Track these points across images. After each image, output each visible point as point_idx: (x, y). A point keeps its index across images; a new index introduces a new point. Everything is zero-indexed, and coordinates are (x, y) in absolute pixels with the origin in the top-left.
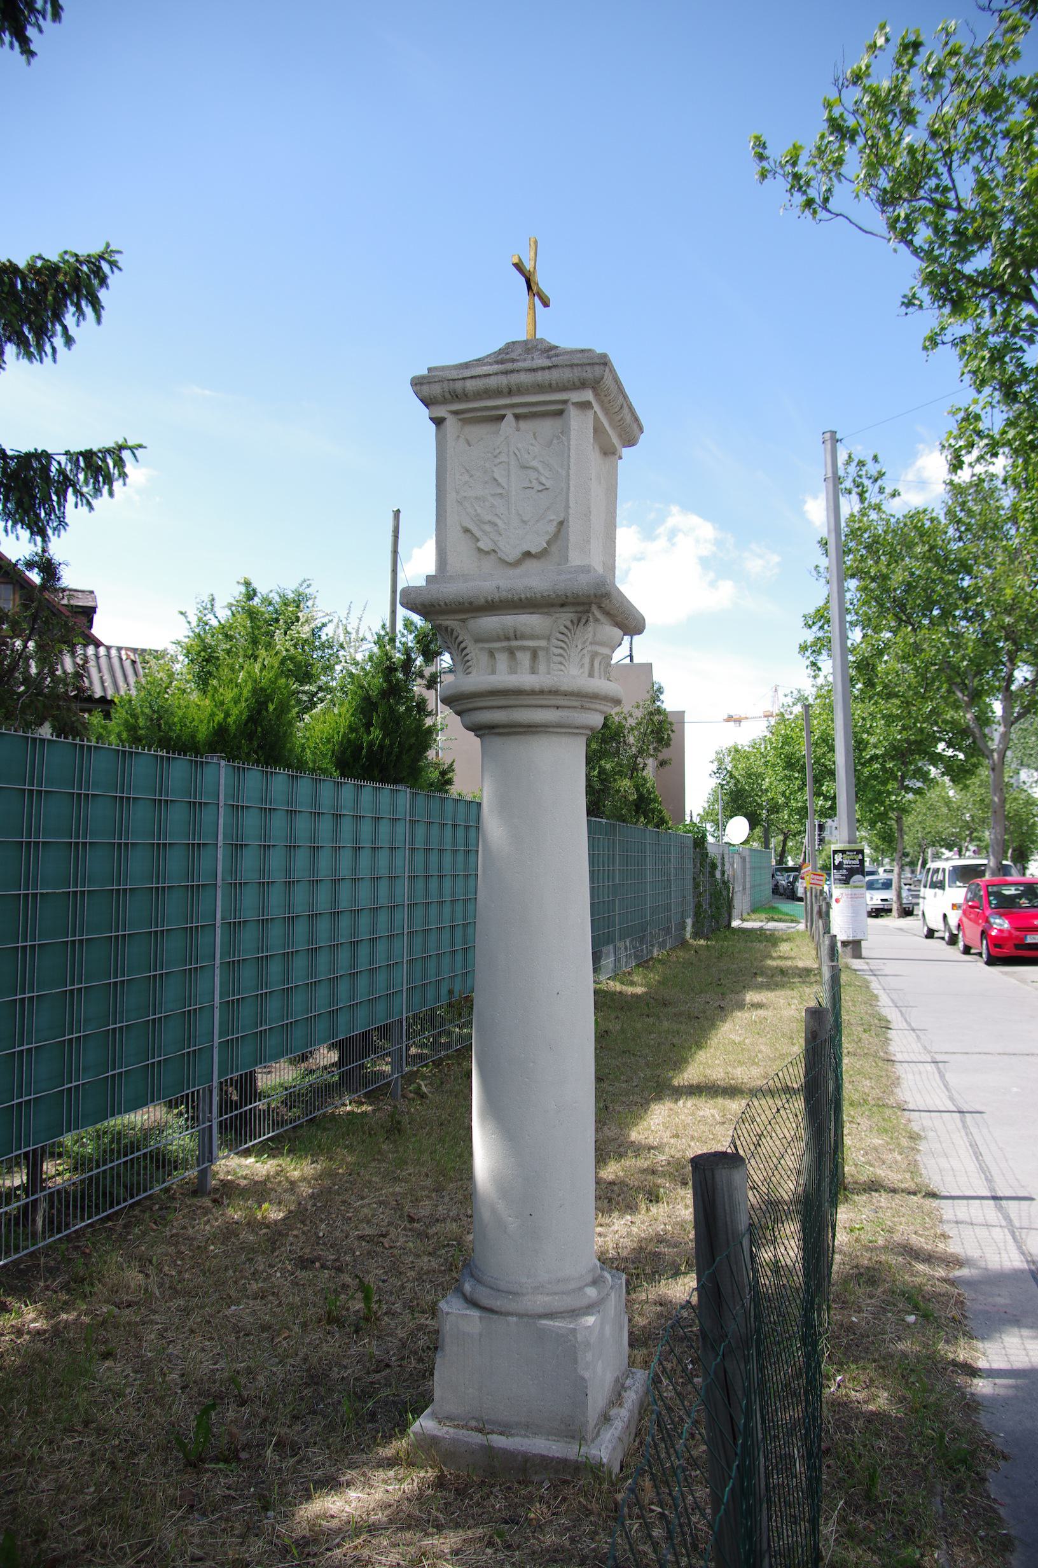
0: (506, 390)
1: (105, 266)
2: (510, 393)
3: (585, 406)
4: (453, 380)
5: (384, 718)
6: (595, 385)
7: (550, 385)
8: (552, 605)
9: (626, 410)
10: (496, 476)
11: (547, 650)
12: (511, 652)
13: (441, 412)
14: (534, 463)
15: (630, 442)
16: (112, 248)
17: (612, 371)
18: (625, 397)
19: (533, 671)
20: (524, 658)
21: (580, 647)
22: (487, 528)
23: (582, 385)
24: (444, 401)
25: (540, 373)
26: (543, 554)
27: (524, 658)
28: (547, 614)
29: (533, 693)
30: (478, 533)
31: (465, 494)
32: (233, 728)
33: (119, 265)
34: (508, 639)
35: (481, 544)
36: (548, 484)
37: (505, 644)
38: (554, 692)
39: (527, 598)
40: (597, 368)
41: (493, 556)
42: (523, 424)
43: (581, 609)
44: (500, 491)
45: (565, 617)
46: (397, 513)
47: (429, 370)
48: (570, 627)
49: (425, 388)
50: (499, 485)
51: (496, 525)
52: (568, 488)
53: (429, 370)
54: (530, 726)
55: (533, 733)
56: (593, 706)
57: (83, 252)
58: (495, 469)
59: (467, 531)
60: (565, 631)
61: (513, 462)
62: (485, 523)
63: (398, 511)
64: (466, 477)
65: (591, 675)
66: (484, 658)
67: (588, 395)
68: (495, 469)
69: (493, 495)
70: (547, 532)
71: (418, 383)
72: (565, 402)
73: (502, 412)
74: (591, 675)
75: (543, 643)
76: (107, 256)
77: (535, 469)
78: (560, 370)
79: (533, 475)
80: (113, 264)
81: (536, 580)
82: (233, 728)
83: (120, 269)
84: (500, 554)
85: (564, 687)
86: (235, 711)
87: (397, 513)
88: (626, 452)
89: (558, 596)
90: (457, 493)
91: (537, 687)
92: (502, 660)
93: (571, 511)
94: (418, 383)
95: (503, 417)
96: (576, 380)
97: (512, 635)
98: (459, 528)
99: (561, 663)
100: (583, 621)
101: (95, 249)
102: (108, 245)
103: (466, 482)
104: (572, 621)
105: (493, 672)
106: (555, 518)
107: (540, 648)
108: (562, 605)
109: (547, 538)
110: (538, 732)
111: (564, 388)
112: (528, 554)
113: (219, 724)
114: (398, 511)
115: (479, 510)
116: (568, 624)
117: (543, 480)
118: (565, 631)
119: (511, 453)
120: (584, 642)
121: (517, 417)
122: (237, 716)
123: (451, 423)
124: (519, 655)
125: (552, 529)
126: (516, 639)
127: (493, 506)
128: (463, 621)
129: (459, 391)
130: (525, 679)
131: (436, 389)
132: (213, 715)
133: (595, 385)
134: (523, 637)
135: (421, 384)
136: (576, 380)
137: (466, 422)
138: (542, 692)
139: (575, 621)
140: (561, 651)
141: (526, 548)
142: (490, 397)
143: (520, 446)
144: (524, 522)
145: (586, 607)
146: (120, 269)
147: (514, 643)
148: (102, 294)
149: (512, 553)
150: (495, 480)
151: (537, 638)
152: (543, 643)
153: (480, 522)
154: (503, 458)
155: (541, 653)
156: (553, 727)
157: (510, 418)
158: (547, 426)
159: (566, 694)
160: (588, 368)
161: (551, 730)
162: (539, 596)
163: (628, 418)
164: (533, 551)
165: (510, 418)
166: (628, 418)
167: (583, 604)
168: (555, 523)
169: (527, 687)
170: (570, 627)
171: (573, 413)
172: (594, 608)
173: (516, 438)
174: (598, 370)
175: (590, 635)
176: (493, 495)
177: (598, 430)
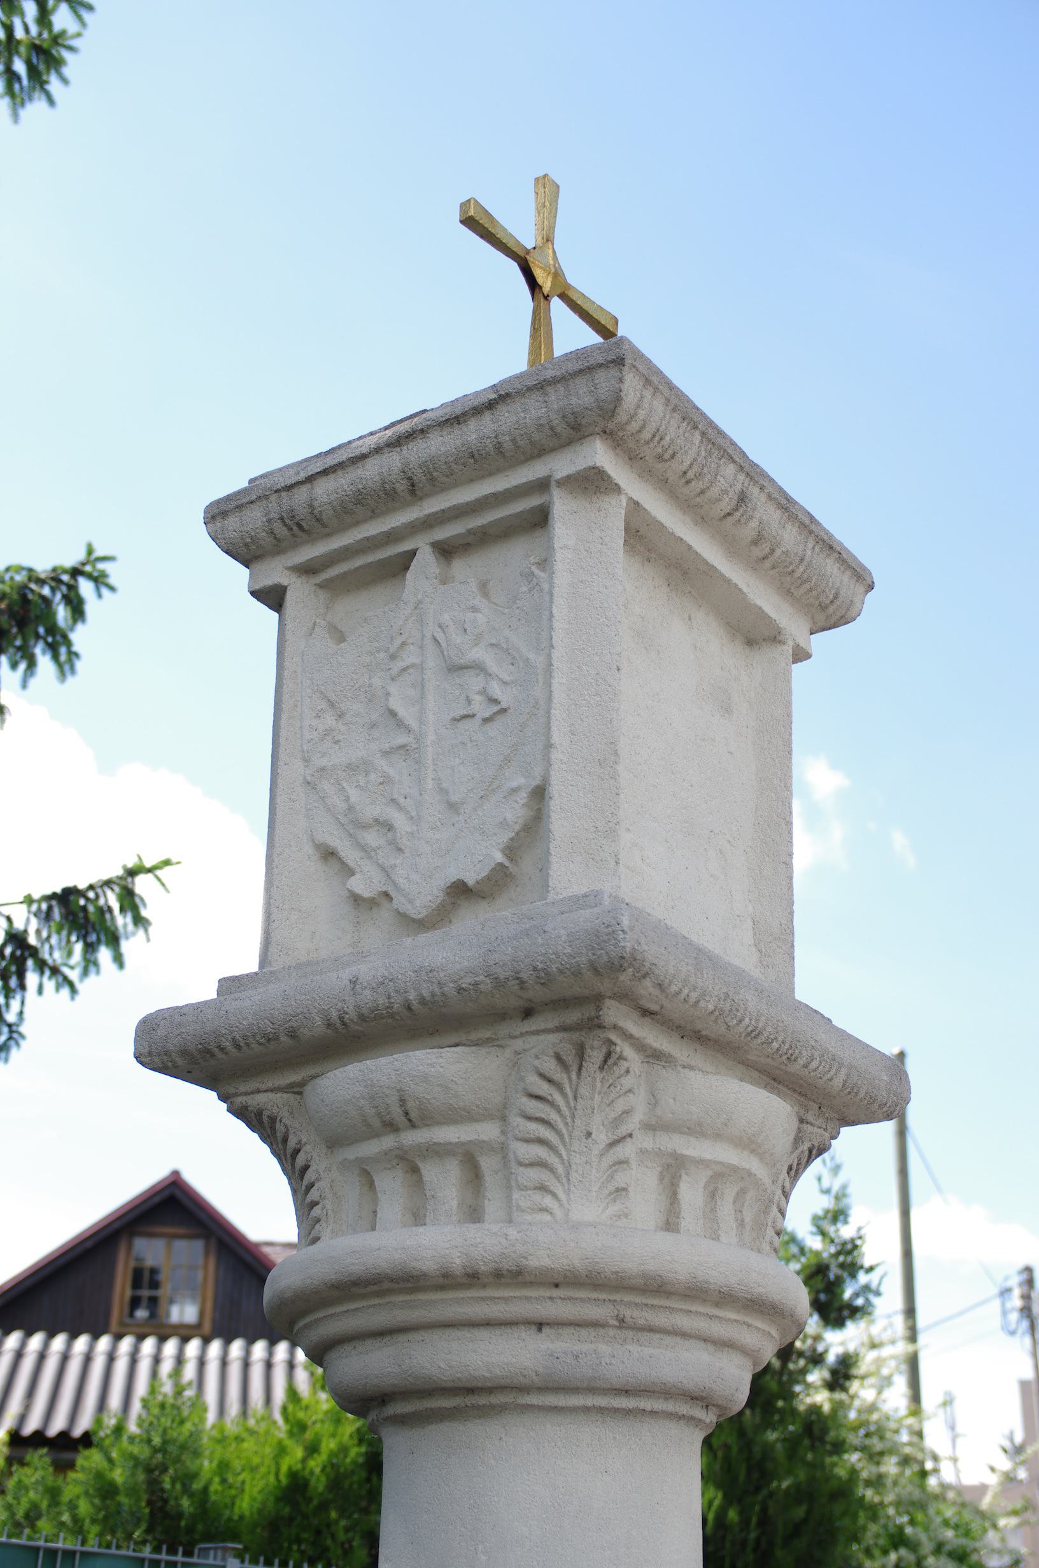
0: (402, 487)
1: (85, 587)
2: (414, 488)
3: (592, 483)
4: (289, 488)
5: (727, 1459)
6: (603, 421)
7: (499, 447)
8: (502, 1016)
9: (765, 513)
10: (395, 704)
11: (502, 1149)
12: (409, 1163)
13: (275, 573)
14: (478, 654)
15: (832, 614)
16: (99, 552)
17: (654, 379)
18: (752, 472)
19: (474, 1214)
20: (444, 1182)
21: (602, 1137)
22: (372, 838)
23: (575, 430)
24: (278, 547)
25: (473, 424)
27: (444, 1182)
29: (447, 1281)
30: (349, 854)
31: (324, 762)
32: (319, 1484)
33: (112, 581)
34: (391, 1127)
35: (357, 884)
36: (506, 697)
37: (388, 1142)
38: (512, 1276)
39: (422, 1001)
40: (601, 376)
41: (384, 914)
42: (459, 567)
43: (573, 1016)
44: (402, 739)
45: (540, 1046)
48: (558, 1075)
49: (233, 522)
50: (400, 724)
51: (390, 827)
52: (550, 699)
54: (471, 1391)
56: (661, 1319)
57: (42, 566)
58: (393, 689)
59: (329, 854)
60: (544, 1088)
62: (365, 827)
64: (330, 720)
65: (670, 1224)
67: (599, 454)
68: (393, 689)
69: (386, 753)
70: (503, 824)
71: (218, 515)
72: (543, 485)
74: (670, 1224)
75: (488, 1131)
76: (90, 570)
77: (478, 667)
78: (517, 405)
79: (475, 682)
80: (99, 580)
81: (454, 955)
82: (319, 1484)
83: (112, 589)
84: (400, 902)
85: (539, 1260)
86: (329, 1445)
88: (820, 643)
89: (499, 984)
90: (306, 761)
91: (457, 1262)
92: (392, 1186)
93: (556, 756)
95: (413, 554)
96: (556, 421)
97: (397, 1113)
98: (309, 849)
99: (543, 1188)
100: (595, 1056)
101: (71, 557)
102: (90, 551)
103: (328, 732)
104: (558, 1058)
106: (521, 781)
107: (481, 1144)
108: (528, 1013)
109: (505, 837)
110: (502, 1409)
111: (539, 452)
112: (460, 891)
113: (293, 1475)
115: (354, 795)
116: (549, 1065)
117: (496, 690)
118: (544, 1088)
119: (428, 641)
120: (617, 1121)
121: (446, 551)
122: (332, 1454)
123: (298, 592)
124: (430, 1172)
125: (515, 812)
126: (413, 1125)
127: (386, 781)
128: (297, 1089)
129: (302, 512)
130: (437, 1240)
131: (255, 518)
132: (281, 1450)
133: (603, 421)
135: (224, 514)
136: (556, 421)
137: (337, 588)
138: (472, 1278)
139: (571, 1059)
140: (541, 1152)
141: (453, 874)
142: (374, 514)
143: (446, 618)
144: (453, 807)
145: (589, 1011)
146: (112, 589)
147: (411, 1138)
148: (80, 637)
149: (422, 892)
150: (393, 714)
152: (488, 1131)
153: (354, 824)
154: (410, 657)
156: (543, 1389)
157: (426, 559)
158: (513, 556)
159: (557, 1281)
161: (534, 1399)
162: (450, 989)
163: (789, 537)
164: (471, 879)
165: (426, 559)
166: (789, 537)
167: (577, 1001)
168: (523, 797)
169: (428, 1265)
170: (558, 1075)
171: (561, 505)
172: (614, 1013)
173: (440, 602)
174: (604, 380)
175: (639, 1102)
176: (386, 753)
177: (640, 536)
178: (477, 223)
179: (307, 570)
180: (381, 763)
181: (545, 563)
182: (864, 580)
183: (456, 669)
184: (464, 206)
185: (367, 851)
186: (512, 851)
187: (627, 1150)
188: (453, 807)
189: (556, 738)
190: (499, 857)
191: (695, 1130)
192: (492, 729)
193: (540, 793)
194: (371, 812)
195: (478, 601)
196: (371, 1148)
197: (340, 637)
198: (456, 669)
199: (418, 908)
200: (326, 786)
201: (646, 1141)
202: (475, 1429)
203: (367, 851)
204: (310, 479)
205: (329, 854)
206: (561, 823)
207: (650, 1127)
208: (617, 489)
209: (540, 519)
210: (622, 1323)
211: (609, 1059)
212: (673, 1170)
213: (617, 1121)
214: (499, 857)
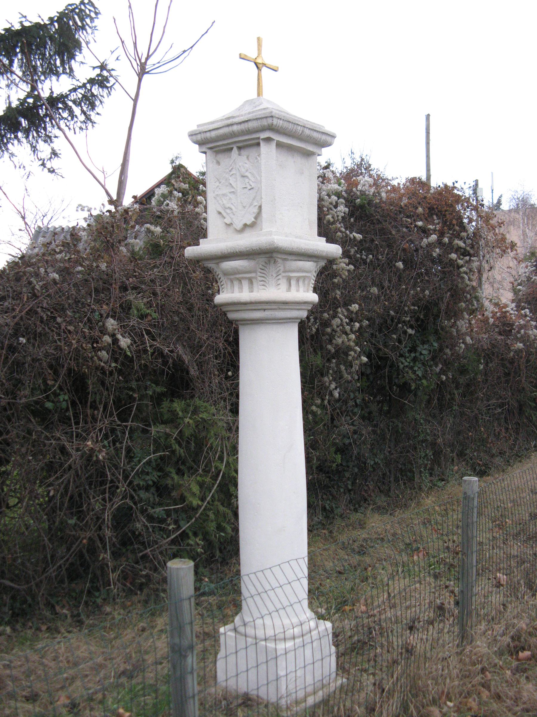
11: (256, 278)
14: (247, 174)
21: (275, 275)
26: (253, 225)
28: (251, 259)
30: (224, 214)
36: (253, 185)
42: (243, 152)
43: (268, 256)
44: (233, 190)
45: (262, 260)
46: (428, 116)
47: (198, 126)
50: (233, 187)
53: (198, 126)
55: (258, 323)
59: (220, 213)
60: (263, 268)
61: (238, 174)
63: (429, 115)
64: (218, 184)
66: (229, 283)
71: (191, 135)
72: (259, 138)
73: (231, 146)
79: (247, 180)
87: (428, 116)
94: (191, 135)
95: (232, 149)
99: (263, 285)
105: (233, 293)
109: (254, 215)
112: (245, 225)
114: (429, 115)
115: (225, 202)
116: (264, 264)
118: (263, 268)
120: (278, 272)
121: (239, 148)
124: (243, 282)
125: (256, 210)
127: (230, 199)
128: (217, 264)
131: (199, 137)
134: (235, 274)
144: (244, 207)
151: (250, 272)
152: (253, 275)
153: (225, 208)
155: (254, 280)
157: (235, 149)
158: (252, 152)
160: (265, 120)
165: (235, 149)
168: (257, 207)
171: (262, 144)
175: (282, 268)
177: (279, 145)
178: (243, 57)
179: (211, 148)
180: (229, 195)
181: (259, 155)
182: (333, 137)
183: (243, 176)
184: (240, 55)
185: (228, 214)
186: (256, 218)
187: (280, 277)
188: (244, 207)
189: (263, 197)
190: (253, 220)
191: (293, 271)
192: (251, 191)
193: (260, 207)
194: (228, 206)
195: (247, 161)
196: (232, 277)
197: (218, 163)
198: (243, 176)
199: (238, 228)
200: (218, 198)
201: (284, 274)
202: (256, 327)
203: (228, 214)
204: (210, 131)
205: (220, 213)
206: (264, 215)
207: (283, 272)
208: (273, 140)
209: (258, 144)
210: (280, 309)
211: (275, 262)
212: (289, 279)
213: (278, 272)
214: (253, 220)
